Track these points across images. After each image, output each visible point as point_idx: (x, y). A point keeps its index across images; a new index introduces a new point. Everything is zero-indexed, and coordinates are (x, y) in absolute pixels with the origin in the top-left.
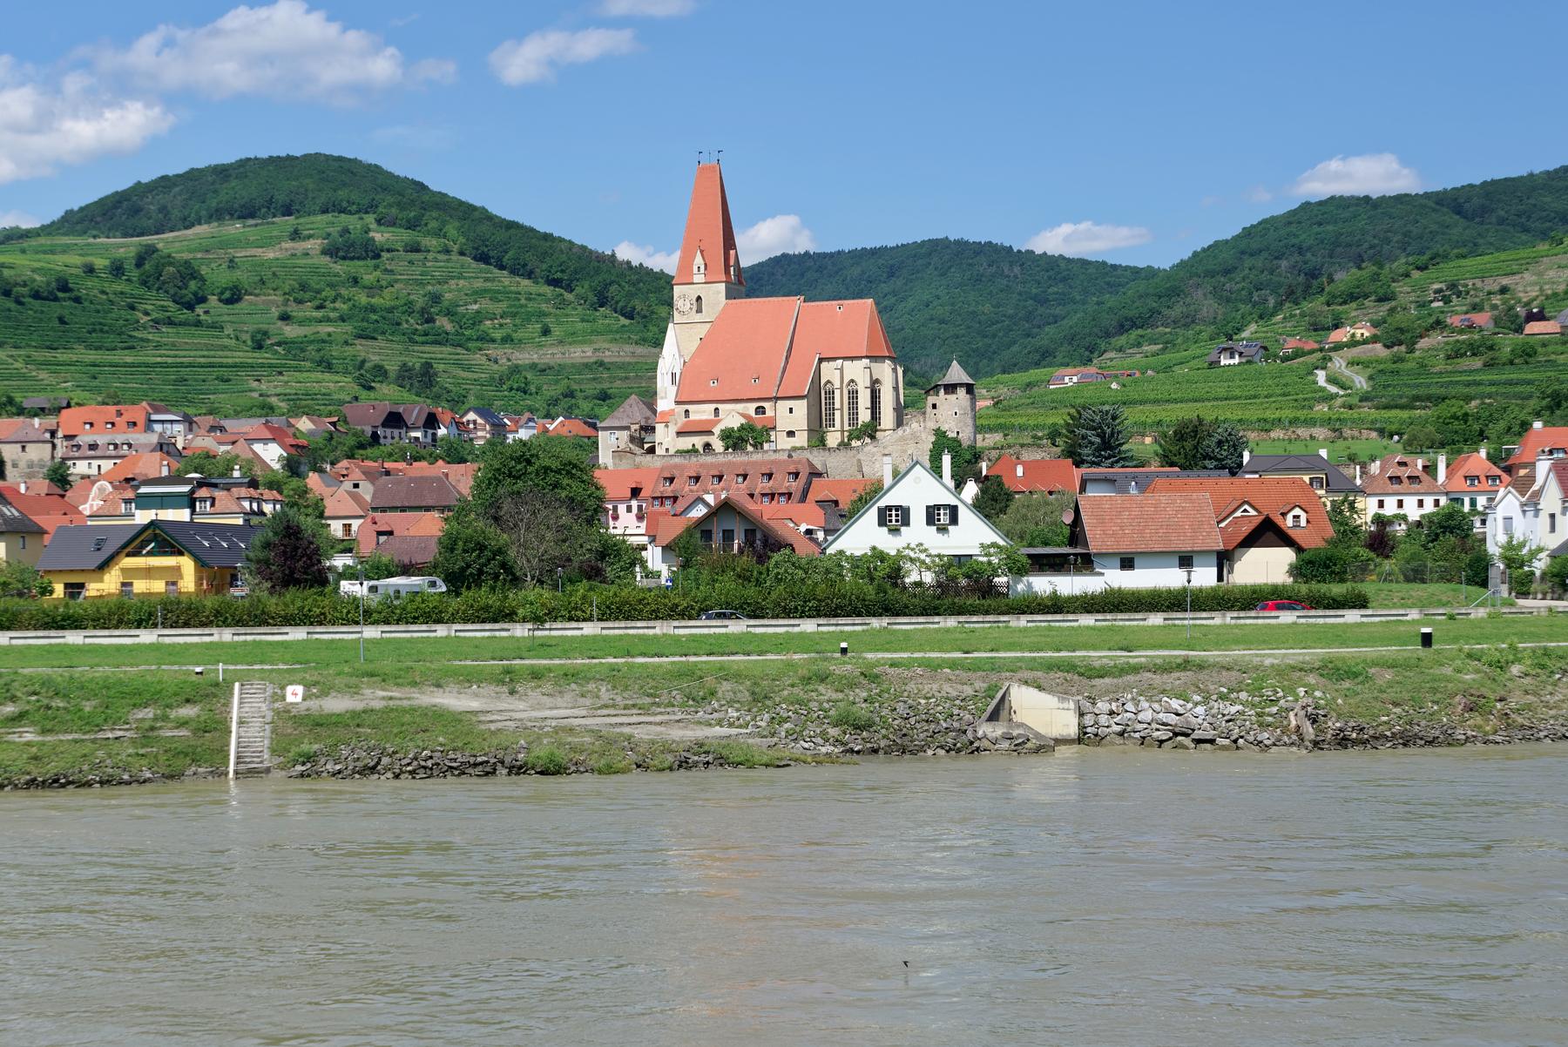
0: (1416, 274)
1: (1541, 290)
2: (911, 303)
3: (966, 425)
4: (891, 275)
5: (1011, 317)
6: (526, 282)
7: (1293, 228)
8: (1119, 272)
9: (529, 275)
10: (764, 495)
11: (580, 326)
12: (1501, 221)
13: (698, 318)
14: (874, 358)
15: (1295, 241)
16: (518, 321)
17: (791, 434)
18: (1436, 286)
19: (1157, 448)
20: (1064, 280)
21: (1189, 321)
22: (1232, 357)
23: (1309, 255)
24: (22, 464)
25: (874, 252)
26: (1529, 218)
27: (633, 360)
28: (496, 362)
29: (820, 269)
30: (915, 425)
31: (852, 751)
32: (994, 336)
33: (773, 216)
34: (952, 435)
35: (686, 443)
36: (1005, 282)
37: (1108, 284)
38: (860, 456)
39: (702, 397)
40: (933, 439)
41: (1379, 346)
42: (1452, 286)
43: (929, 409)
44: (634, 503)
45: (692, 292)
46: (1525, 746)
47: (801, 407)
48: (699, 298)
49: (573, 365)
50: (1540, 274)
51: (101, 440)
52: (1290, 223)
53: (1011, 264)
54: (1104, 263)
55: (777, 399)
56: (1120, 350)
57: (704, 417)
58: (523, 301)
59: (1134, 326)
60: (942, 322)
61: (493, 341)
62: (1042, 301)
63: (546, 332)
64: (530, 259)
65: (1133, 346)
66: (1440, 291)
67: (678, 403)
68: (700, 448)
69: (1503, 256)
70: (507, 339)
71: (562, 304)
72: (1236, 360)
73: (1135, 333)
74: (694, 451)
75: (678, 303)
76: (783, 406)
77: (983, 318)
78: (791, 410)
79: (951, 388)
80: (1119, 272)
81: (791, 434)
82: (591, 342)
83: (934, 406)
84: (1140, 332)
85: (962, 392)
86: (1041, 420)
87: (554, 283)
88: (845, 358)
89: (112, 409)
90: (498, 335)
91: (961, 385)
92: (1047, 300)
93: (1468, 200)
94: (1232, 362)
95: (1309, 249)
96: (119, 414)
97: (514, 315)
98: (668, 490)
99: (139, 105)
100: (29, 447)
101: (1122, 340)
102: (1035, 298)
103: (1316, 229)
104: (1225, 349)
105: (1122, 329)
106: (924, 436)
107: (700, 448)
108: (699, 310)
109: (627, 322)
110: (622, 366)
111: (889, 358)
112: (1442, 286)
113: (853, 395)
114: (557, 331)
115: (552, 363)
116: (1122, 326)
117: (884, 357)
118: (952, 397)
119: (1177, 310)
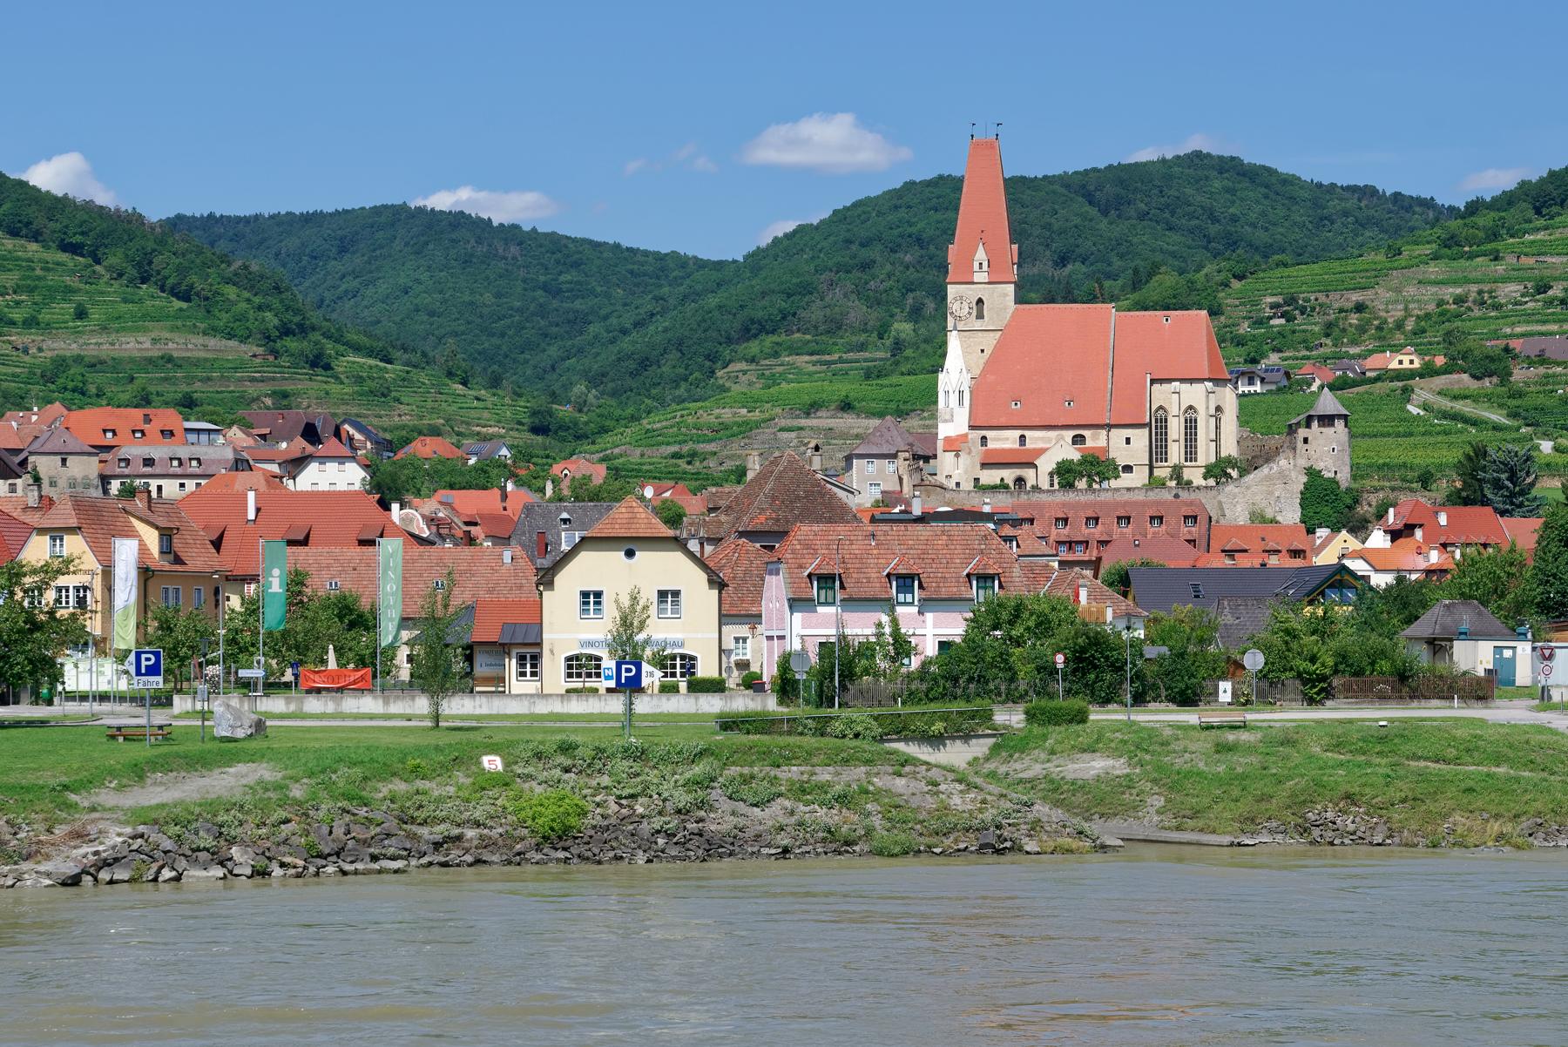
0: (1236, 284)
2: (383, 288)
3: (1344, 464)
4: (343, 250)
5: (520, 310)
6: (34, 246)
7: (902, 213)
9: (36, 237)
10: (1059, 543)
11: (124, 307)
12: (1142, 216)
13: (978, 325)
14: (1218, 382)
15: (913, 230)
16: (38, 299)
17: (1128, 469)
18: (1270, 300)
20: (576, 265)
21: (835, 326)
22: (1251, 382)
23: (932, 247)
24: (62, 483)
25: (311, 219)
27: (202, 355)
28: (26, 351)
29: (236, 238)
30: (1283, 462)
31: (1104, 847)
32: (503, 335)
33: (49, 159)
34: (1328, 475)
35: (991, 477)
36: (502, 264)
37: (631, 272)
38: (1221, 498)
39: (1003, 421)
40: (1305, 479)
42: (1291, 300)
43: (1300, 444)
45: (972, 293)
46: (1457, 851)
47: (1141, 438)
48: (980, 301)
49: (132, 360)
50: (1398, 290)
51: (159, 452)
53: (506, 242)
54: (617, 246)
55: (1110, 427)
56: (753, 360)
57: (1007, 445)
58: (38, 272)
60: (432, 314)
61: (13, 323)
63: (81, 314)
64: (39, 221)
67: (972, 427)
68: (1010, 481)
70: (30, 323)
71: (92, 279)
72: (1258, 388)
73: (769, 340)
74: (1002, 486)
75: (954, 306)
76: (1119, 435)
77: (486, 311)
78: (1128, 441)
79: (1327, 420)
80: (639, 258)
81: (1128, 469)
82: (146, 330)
83: (1306, 441)
84: (775, 338)
85: (1339, 424)
86: (1407, 457)
87: (74, 249)
88: (1182, 381)
89: (138, 414)
90: (17, 315)
91: (1340, 416)
92: (560, 291)
93: (1099, 188)
94: (1252, 389)
95: (931, 240)
96: (147, 419)
97: (31, 290)
100: (70, 459)
101: (753, 347)
102: (545, 287)
104: (1243, 373)
105: (752, 329)
106: (1293, 474)
107: (1010, 481)
108: (980, 316)
109: (184, 305)
110: (197, 363)
111: (1209, 380)
112: (1279, 299)
113: (1191, 426)
114: (96, 314)
115: (103, 355)
116: (748, 330)
118: (1328, 431)
119: (815, 313)
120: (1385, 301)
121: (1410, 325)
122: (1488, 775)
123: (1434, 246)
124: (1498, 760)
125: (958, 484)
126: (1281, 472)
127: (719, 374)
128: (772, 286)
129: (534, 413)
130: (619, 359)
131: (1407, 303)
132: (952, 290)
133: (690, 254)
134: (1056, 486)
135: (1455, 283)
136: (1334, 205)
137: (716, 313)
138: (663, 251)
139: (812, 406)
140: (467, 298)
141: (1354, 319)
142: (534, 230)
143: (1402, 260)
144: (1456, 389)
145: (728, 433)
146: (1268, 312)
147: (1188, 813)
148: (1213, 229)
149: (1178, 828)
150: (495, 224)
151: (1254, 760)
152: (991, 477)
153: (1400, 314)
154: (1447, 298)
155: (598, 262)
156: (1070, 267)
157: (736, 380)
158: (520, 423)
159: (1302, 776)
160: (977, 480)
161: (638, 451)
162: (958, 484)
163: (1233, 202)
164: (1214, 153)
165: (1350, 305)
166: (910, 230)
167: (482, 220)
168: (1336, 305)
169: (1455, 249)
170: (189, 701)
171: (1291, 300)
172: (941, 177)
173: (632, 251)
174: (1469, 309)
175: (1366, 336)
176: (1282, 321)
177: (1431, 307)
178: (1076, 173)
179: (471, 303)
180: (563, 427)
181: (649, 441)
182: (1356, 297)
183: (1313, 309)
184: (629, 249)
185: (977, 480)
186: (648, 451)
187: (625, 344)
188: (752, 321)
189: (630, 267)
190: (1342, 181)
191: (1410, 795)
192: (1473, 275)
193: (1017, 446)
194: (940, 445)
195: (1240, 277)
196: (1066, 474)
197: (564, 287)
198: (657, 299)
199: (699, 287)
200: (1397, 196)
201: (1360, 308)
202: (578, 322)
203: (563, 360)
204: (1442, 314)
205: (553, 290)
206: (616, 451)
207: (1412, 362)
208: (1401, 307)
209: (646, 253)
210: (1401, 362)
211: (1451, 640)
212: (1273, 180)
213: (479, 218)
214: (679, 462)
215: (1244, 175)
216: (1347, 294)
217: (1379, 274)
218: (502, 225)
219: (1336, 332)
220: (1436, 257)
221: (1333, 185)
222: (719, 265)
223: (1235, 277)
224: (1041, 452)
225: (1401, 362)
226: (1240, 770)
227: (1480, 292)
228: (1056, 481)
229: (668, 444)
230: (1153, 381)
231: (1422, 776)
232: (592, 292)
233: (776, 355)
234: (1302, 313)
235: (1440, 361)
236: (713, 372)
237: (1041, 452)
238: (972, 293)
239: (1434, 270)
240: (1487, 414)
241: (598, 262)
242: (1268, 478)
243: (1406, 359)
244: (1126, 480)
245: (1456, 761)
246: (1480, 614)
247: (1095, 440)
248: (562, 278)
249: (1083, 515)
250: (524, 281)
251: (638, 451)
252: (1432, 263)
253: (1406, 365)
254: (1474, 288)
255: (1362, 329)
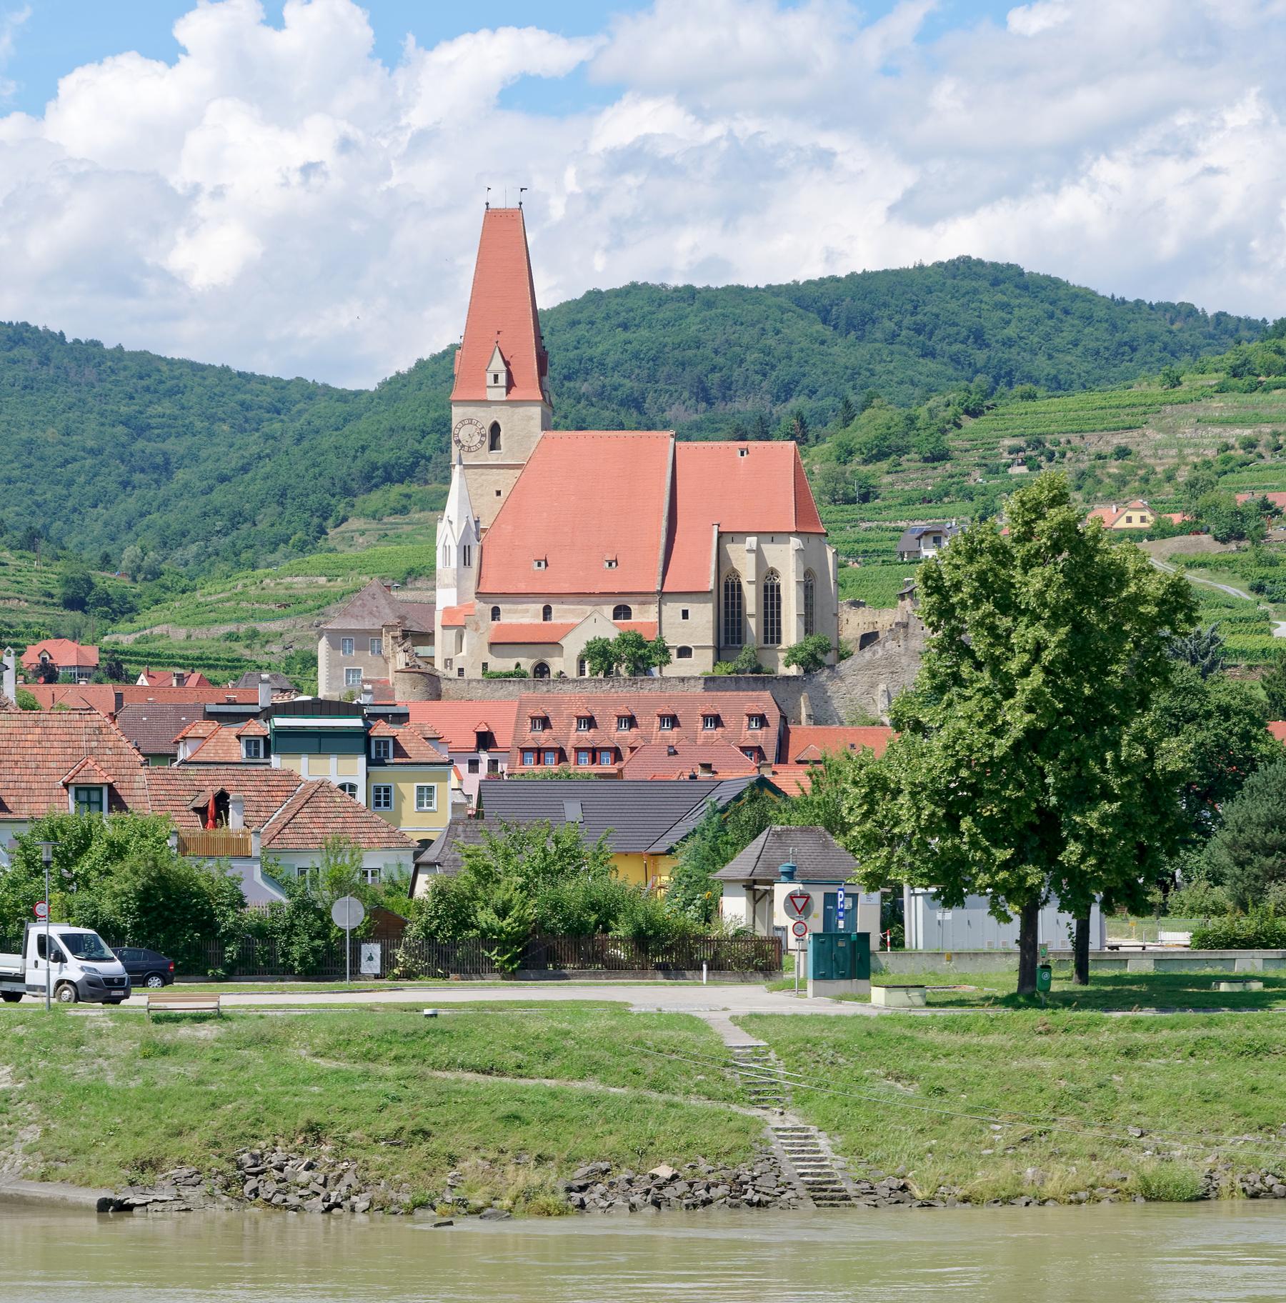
0: (969, 423)
1: (1181, 456)
7: (581, 330)
8: (254, 386)
13: (493, 458)
17: (684, 652)
18: (1008, 442)
19: (25, 666)
20: (171, 393)
26: (931, 334)
37: (242, 404)
41: (1205, 538)
44: (484, 757)
50: (1171, 430)
52: (574, 324)
54: (226, 370)
57: (526, 620)
59: (388, 479)
62: (140, 430)
65: (395, 512)
66: (1014, 450)
69: (1097, 398)
74: (518, 674)
76: (673, 610)
77: (48, 451)
78: (685, 614)
81: (684, 652)
98: (543, 738)
99: (372, 32)
100: (513, 668)
101: (375, 499)
103: (621, 335)
106: (904, 661)
108: (494, 446)
111: (797, 534)
112: (1021, 442)
117: (790, 533)
120: (1149, 442)
121: (1183, 475)
122: (553, 1095)
123: (1222, 375)
124: (591, 1069)
125: (461, 671)
126: (888, 657)
127: (332, 533)
128: (402, 422)
129: (68, 582)
130: (205, 514)
131: (1181, 447)
132: (457, 413)
133: (320, 381)
134: (587, 674)
135: (1243, 422)
136: (1139, 328)
137: (331, 456)
138: (286, 378)
139: (410, 572)
140: (25, 435)
141: (1114, 468)
142: (120, 348)
143: (1180, 393)
144: (1192, 556)
145: (301, 607)
146: (1007, 458)
147: (65, 1153)
148: (980, 357)
149: (44, 1178)
150: (69, 340)
151: (192, 1070)
152: (504, 664)
153: (1170, 462)
154: (1232, 441)
155: (199, 390)
156: (793, 401)
157: (350, 542)
158: (51, 596)
159: (249, 1095)
160: (485, 665)
161: (182, 633)
162: (461, 671)
163: (1008, 322)
164: (986, 259)
165: (1108, 450)
166: (589, 352)
167: (52, 335)
168: (1093, 450)
169: (1248, 379)
170: (1277, 924)
171: (1038, 443)
172: (634, 286)
173: (245, 377)
174: (1261, 456)
175: (1126, 490)
176: (1024, 469)
177: (1210, 454)
178: (809, 282)
179: (31, 442)
180: (106, 600)
181: (199, 619)
182: (1119, 440)
183: (1063, 455)
184: (240, 374)
185: (485, 665)
186: (198, 632)
187: (217, 497)
188: (375, 467)
189: (240, 397)
190: (1152, 297)
191: (410, 1125)
192: (1265, 413)
193: (540, 620)
194: (438, 618)
195: (974, 413)
196: (601, 657)
197: (153, 422)
198: (268, 437)
199: (317, 423)
200: (1221, 317)
201: (1123, 453)
202: (165, 468)
203: (142, 515)
204: (1225, 462)
205: (140, 430)
206: (157, 631)
207: (1143, 519)
208: (1173, 452)
209: (264, 380)
210: (1129, 520)
211: (771, 883)
212: (1061, 293)
213: (46, 331)
214: (235, 645)
215: (1026, 288)
216: (1107, 436)
217: (1150, 408)
218: (77, 341)
219: (1089, 483)
220: (1222, 389)
221: (1139, 303)
222: (344, 397)
223: (967, 412)
224: (570, 628)
225: (1129, 520)
226: (162, 1085)
227: (1275, 434)
228: (587, 666)
229: (224, 621)
230: (720, 534)
231: (444, 1097)
232: (189, 429)
233: (404, 510)
234: (1050, 459)
235: (1177, 518)
236: (322, 531)
237: (570, 628)
238: (486, 417)
239: (1218, 406)
240: (1223, 587)
241: (199, 390)
242: (870, 665)
243: (1136, 516)
244: (677, 667)
245: (520, 1070)
246: (826, 846)
247: (643, 616)
248: (150, 411)
249: (613, 712)
250: (102, 415)
251: (182, 633)
252: (1218, 396)
253: (1136, 523)
254: (1267, 429)
255: (1122, 481)
